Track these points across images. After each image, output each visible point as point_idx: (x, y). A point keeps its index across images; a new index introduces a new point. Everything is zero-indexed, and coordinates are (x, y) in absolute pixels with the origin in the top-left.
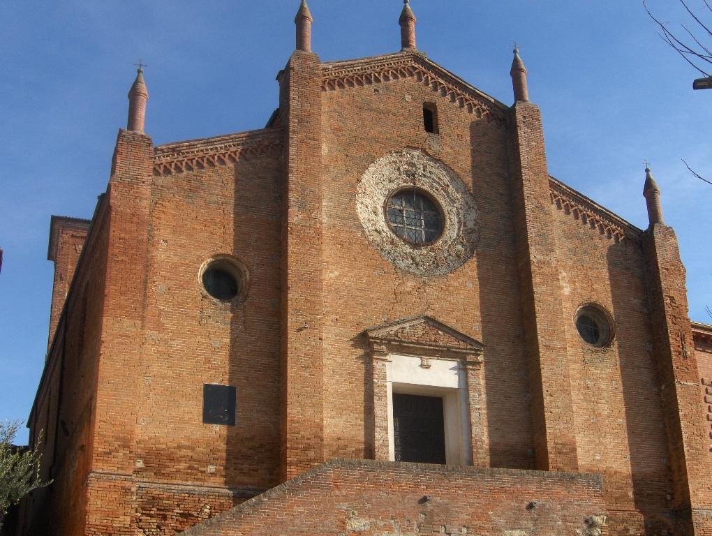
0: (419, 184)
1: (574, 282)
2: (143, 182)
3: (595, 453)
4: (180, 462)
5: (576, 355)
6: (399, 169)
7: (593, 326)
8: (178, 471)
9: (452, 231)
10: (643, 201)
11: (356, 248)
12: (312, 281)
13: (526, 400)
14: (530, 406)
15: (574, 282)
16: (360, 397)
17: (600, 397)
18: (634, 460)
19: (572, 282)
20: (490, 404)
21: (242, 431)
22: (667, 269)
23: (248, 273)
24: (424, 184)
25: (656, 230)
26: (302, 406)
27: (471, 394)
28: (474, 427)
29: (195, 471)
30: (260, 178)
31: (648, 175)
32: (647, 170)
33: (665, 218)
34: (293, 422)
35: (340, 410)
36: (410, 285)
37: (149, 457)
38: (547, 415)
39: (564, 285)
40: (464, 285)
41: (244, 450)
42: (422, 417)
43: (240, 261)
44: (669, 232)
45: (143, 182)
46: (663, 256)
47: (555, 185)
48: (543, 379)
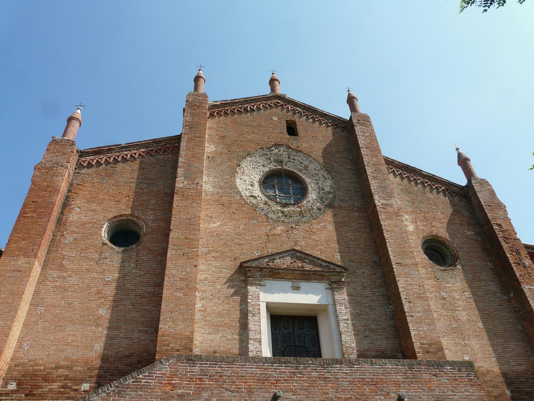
0: (285, 167)
1: (416, 222)
2: (62, 166)
3: (463, 354)
4: (54, 381)
5: (427, 273)
6: (270, 159)
7: (437, 251)
8: (51, 390)
9: (312, 195)
10: (460, 169)
11: (235, 206)
12: (192, 225)
13: (389, 311)
14: (394, 315)
15: (416, 222)
16: (236, 315)
17: (456, 305)
18: (500, 359)
19: (414, 222)
20: (355, 316)
21: (121, 349)
22: (490, 206)
23: (144, 227)
24: (289, 167)
25: (473, 182)
26: (174, 321)
27: (338, 308)
28: (341, 333)
29: (68, 390)
30: (161, 166)
31: (458, 152)
32: (457, 149)
33: (479, 172)
34: (164, 335)
35: (216, 328)
36: (279, 229)
37: (23, 378)
38: (409, 319)
39: (408, 224)
40: (325, 227)
41: (121, 367)
42: (296, 333)
43: (139, 219)
44: (484, 183)
45: (62, 166)
46: (483, 197)
47: (389, 162)
48: (400, 289)
